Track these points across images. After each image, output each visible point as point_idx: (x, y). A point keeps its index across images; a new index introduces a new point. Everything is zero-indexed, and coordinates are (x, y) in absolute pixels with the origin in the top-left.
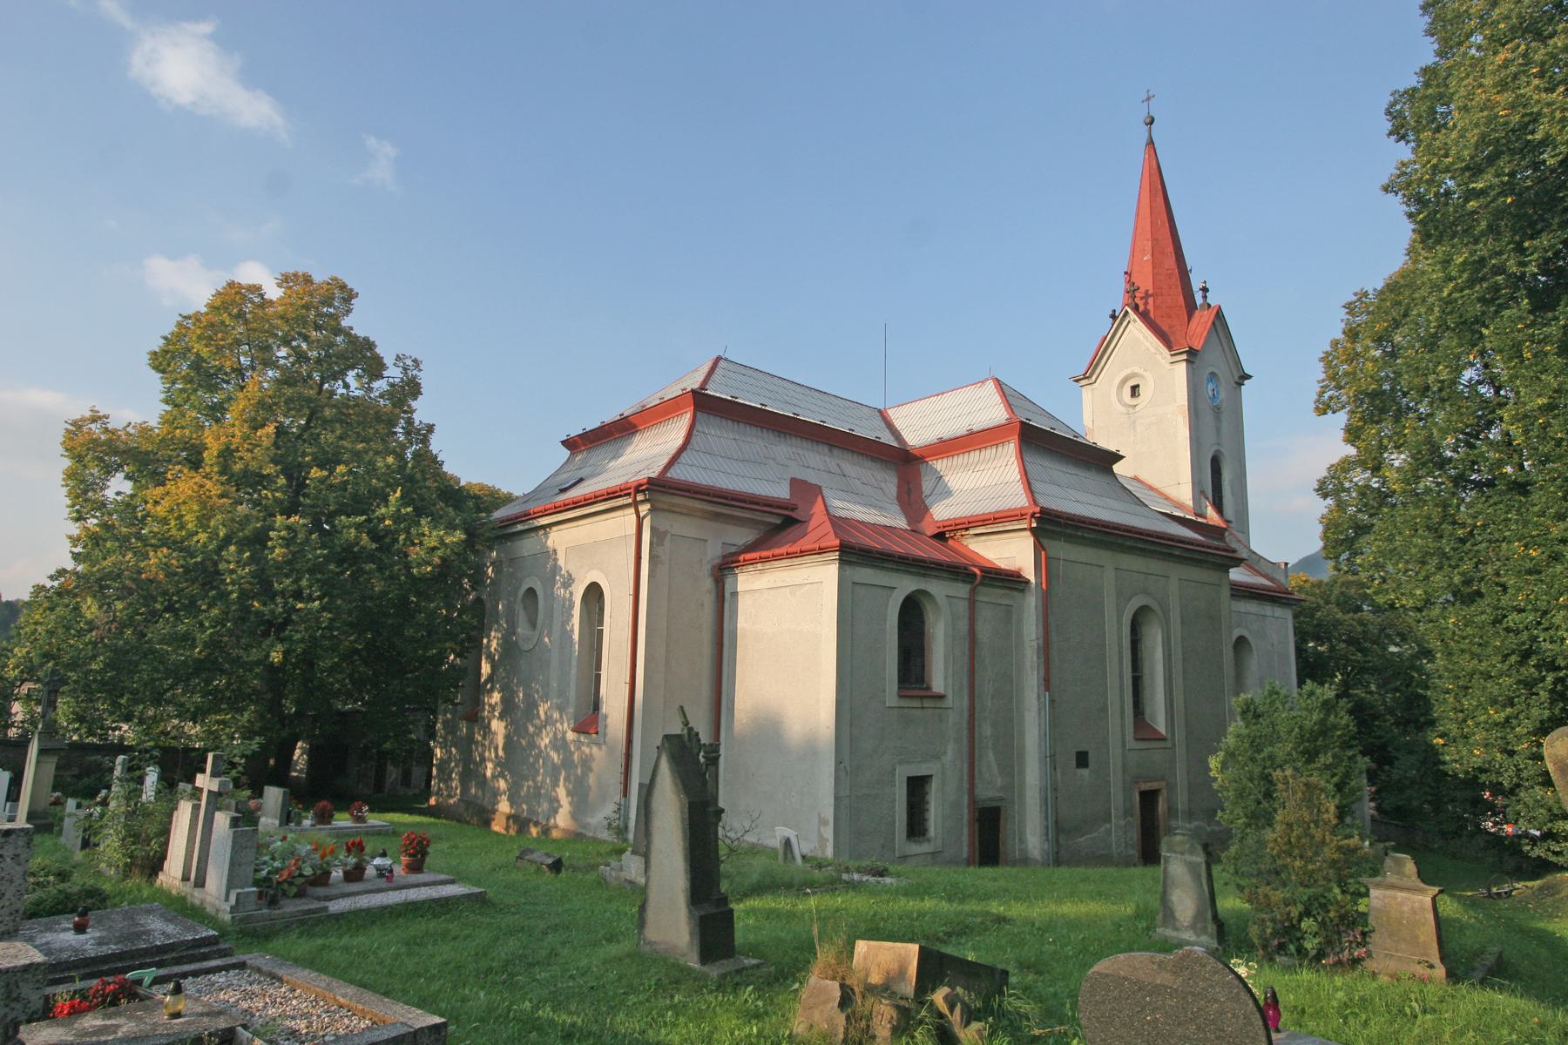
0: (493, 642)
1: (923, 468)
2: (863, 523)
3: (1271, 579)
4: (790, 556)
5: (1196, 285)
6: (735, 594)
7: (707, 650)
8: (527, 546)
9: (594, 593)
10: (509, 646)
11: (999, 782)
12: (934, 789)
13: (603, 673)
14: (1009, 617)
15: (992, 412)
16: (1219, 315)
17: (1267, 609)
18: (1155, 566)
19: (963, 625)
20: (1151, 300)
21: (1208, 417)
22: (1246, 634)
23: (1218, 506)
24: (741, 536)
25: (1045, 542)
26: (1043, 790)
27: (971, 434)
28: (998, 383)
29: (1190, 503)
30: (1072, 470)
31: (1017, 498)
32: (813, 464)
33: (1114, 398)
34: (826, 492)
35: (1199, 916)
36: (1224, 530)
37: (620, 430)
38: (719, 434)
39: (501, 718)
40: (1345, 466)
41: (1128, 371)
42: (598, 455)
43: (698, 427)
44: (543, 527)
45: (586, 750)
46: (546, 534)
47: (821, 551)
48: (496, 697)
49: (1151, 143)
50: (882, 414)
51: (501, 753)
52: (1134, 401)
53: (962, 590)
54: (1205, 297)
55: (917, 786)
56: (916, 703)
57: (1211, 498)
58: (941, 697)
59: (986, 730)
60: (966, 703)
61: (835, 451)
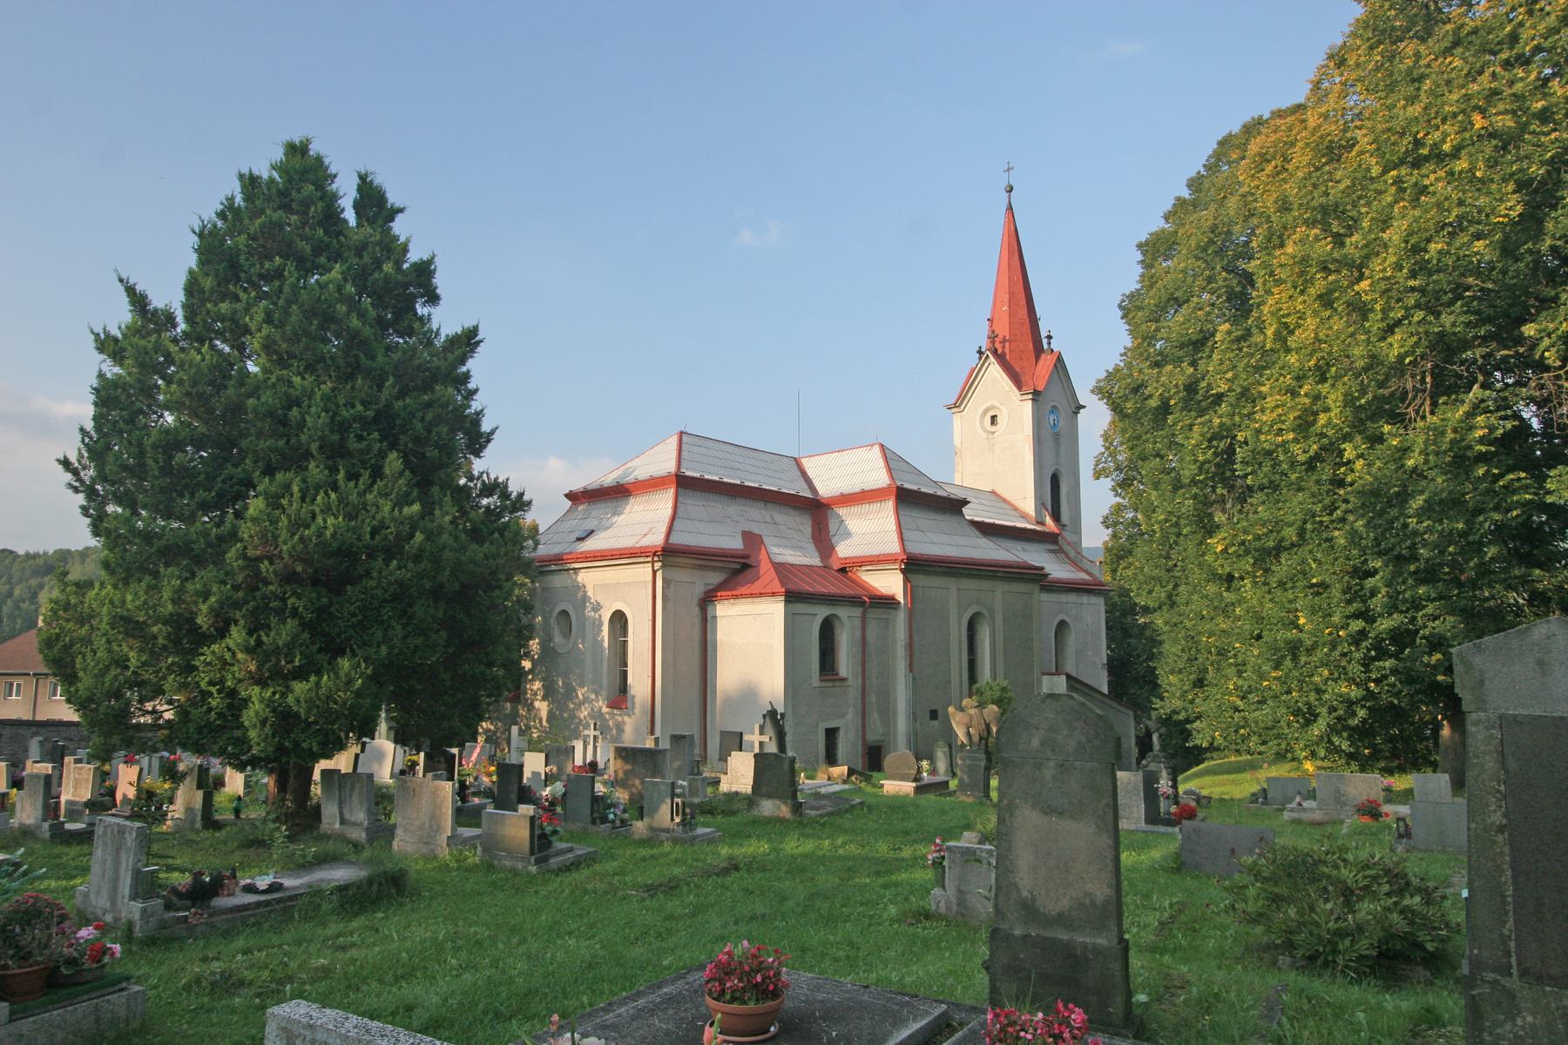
0: (534, 645)
1: (829, 512)
2: (792, 565)
3: (1090, 574)
4: (752, 595)
5: (1044, 334)
6: (715, 617)
7: (697, 653)
8: (558, 581)
9: (619, 619)
10: (546, 649)
11: (881, 730)
12: (841, 734)
13: (630, 669)
14: (887, 625)
15: (878, 477)
16: (1060, 359)
17: (1085, 599)
18: (984, 584)
19: (858, 633)
20: (1007, 344)
21: (1049, 443)
22: (1067, 619)
23: (1056, 516)
24: (715, 578)
25: (911, 577)
26: (908, 734)
27: (863, 492)
28: (882, 446)
29: (1033, 513)
30: (933, 516)
31: (894, 547)
32: (756, 518)
33: (978, 424)
34: (766, 540)
35: (946, 771)
36: (1057, 535)
37: (618, 493)
38: (696, 505)
39: (544, 699)
40: (1118, 509)
41: (989, 404)
42: (599, 510)
43: (680, 499)
44: (574, 569)
45: (620, 719)
46: (576, 574)
47: (773, 594)
48: (537, 685)
49: (1010, 208)
50: (797, 461)
51: (545, 723)
52: (993, 429)
53: (857, 612)
54: (1049, 343)
55: (831, 734)
56: (830, 684)
57: (1049, 507)
58: (844, 680)
59: (872, 698)
60: (860, 682)
61: (769, 505)
